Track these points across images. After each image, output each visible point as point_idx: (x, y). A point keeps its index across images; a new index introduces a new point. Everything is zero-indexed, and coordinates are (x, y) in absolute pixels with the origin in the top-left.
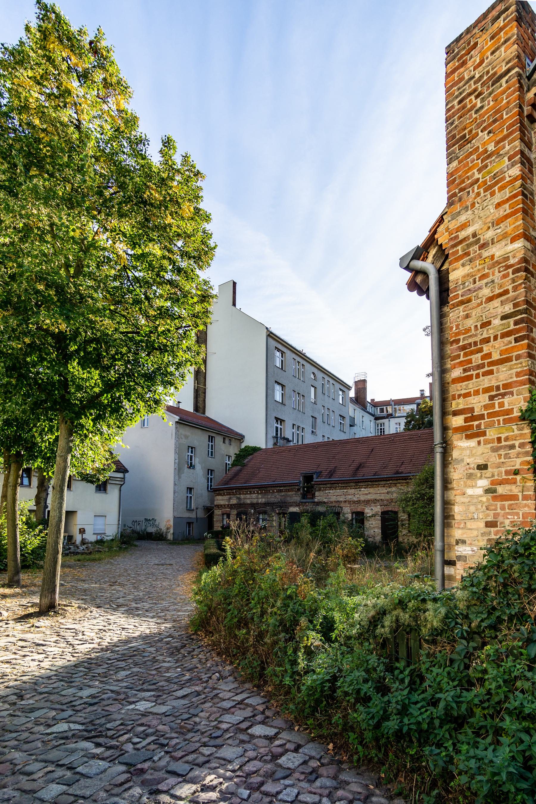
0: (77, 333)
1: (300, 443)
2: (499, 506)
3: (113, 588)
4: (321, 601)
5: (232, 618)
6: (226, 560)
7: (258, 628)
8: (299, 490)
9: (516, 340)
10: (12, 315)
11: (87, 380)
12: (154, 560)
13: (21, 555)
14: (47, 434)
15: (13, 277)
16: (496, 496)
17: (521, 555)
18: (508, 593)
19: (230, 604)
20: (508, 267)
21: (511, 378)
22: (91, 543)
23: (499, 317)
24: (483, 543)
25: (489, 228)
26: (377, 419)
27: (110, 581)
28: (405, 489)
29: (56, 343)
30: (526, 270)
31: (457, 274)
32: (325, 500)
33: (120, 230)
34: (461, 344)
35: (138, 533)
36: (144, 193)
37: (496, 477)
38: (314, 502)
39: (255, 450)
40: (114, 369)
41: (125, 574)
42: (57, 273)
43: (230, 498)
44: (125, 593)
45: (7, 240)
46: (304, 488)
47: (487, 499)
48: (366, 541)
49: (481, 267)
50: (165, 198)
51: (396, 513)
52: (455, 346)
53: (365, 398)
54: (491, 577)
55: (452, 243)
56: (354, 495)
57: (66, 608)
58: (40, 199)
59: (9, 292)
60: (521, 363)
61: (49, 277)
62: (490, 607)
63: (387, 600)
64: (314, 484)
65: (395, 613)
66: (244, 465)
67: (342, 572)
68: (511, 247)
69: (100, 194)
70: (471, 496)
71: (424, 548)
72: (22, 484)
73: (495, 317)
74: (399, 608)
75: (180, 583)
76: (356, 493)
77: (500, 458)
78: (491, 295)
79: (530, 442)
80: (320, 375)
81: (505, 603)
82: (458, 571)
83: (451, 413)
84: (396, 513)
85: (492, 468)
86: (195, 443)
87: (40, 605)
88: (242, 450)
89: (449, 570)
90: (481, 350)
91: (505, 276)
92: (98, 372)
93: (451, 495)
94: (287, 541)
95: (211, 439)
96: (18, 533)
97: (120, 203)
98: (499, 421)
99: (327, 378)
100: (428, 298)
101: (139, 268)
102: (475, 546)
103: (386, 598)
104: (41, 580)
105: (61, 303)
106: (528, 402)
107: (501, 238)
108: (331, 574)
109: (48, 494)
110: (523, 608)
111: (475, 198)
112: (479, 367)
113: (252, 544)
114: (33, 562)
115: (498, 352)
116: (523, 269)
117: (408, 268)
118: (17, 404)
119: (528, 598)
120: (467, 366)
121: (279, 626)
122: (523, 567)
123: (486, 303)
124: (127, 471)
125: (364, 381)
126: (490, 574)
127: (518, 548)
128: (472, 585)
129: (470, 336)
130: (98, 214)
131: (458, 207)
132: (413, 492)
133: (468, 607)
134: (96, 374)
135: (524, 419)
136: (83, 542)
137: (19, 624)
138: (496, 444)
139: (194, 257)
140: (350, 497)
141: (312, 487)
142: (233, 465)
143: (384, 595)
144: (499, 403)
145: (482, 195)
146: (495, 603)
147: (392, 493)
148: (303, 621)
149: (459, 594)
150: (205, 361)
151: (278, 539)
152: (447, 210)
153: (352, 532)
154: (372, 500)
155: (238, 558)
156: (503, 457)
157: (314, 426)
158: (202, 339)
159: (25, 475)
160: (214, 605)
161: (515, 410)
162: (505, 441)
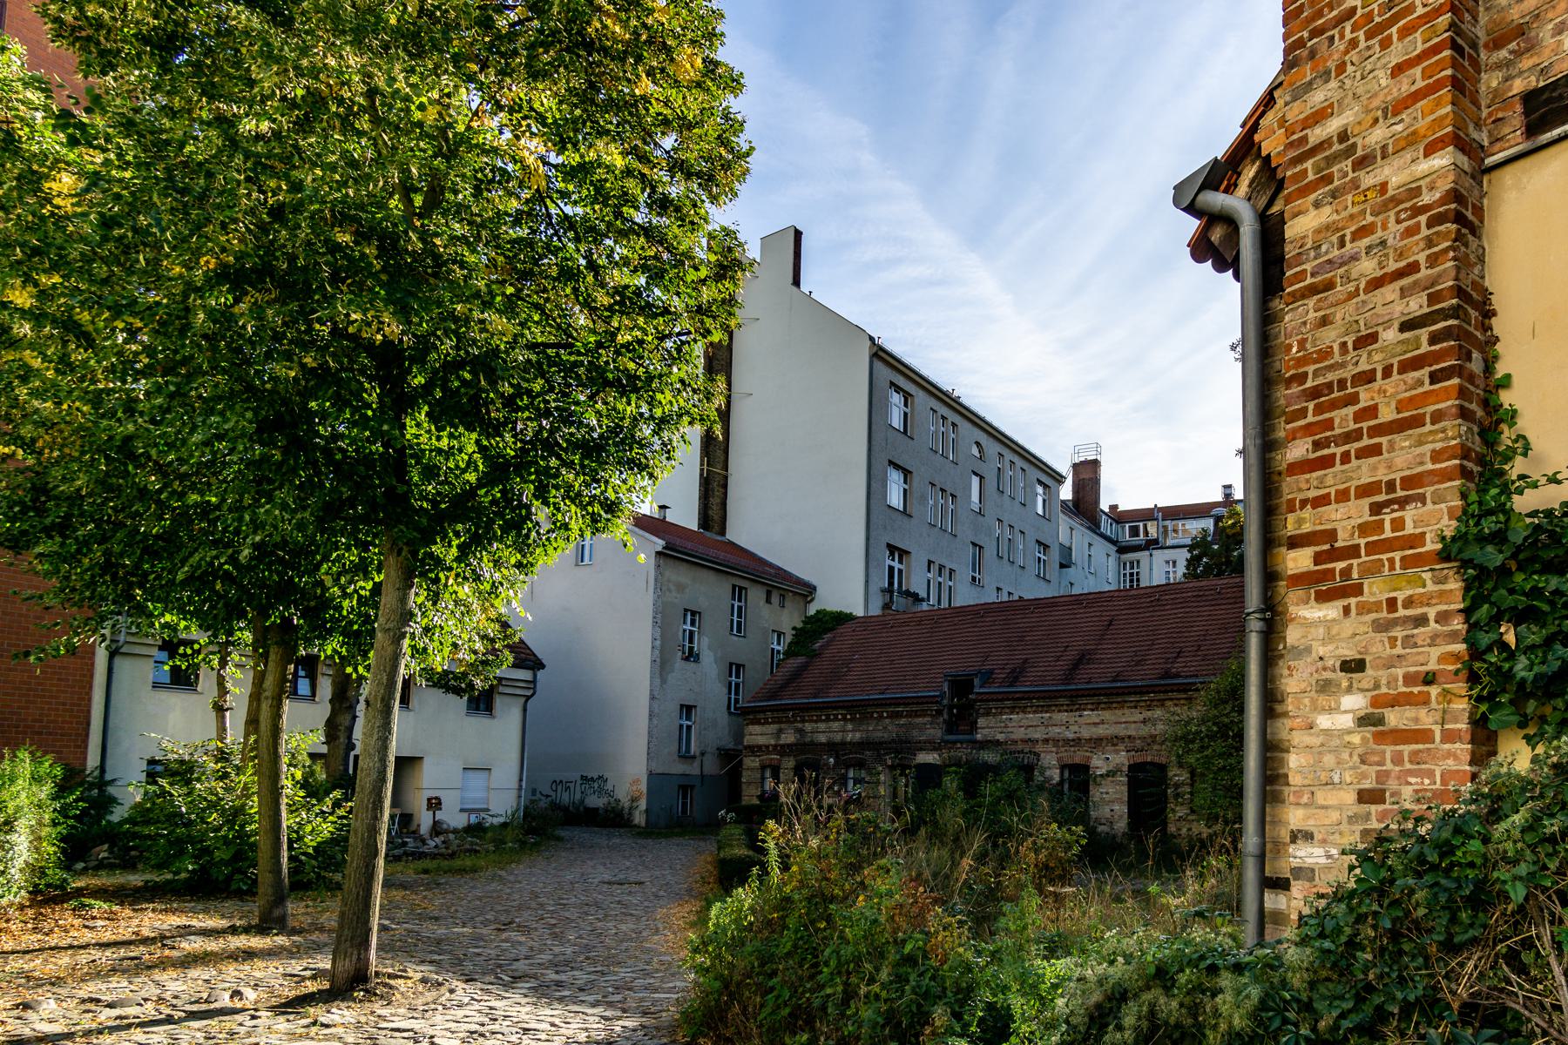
0: (424, 346)
1: (944, 604)
2: (1388, 756)
3: (504, 935)
4: (982, 969)
5: (779, 1007)
6: (768, 874)
7: (837, 1030)
8: (939, 712)
9: (1434, 378)
10: (275, 301)
11: (448, 454)
12: (599, 872)
13: (291, 858)
14: (351, 579)
15: (278, 212)
16: (1382, 733)
17: (1434, 868)
18: (1401, 953)
19: (774, 974)
20: (1417, 211)
21: (1422, 463)
22: (455, 831)
23: (1396, 325)
24: (1352, 837)
25: (1376, 121)
26: (1123, 550)
27: (496, 921)
28: (1184, 712)
29: (378, 369)
30: (1459, 218)
31: (1303, 224)
32: (1001, 737)
33: (532, 109)
34: (1309, 384)
35: (565, 809)
36: (589, 23)
37: (1384, 690)
38: (976, 742)
39: (842, 618)
40: (514, 428)
41: (534, 905)
42: (382, 206)
43: (780, 731)
44: (531, 948)
45: (265, 126)
46: (951, 707)
47: (1363, 739)
48: (1091, 832)
49: (1356, 209)
50: (636, 34)
51: (1163, 768)
52: (1295, 389)
53: (1097, 501)
54: (1366, 916)
55: (1292, 154)
56: (1067, 725)
57: (392, 982)
58: (344, 32)
59: (271, 249)
60: (1444, 431)
61: (364, 216)
62: (1360, 985)
63: (1131, 968)
64: (975, 701)
65: (1147, 997)
66: (815, 655)
67: (1032, 901)
68: (1424, 166)
69: (486, 24)
70: (1326, 732)
71: (1223, 850)
72: (295, 692)
73: (1387, 324)
74: (1156, 986)
75: (660, 926)
76: (1072, 720)
77: (1393, 646)
78: (1379, 273)
79: (1460, 611)
80: (992, 448)
81: (1394, 975)
82: (1294, 902)
83: (1284, 541)
84: (1163, 768)
85: (1376, 668)
86: (701, 603)
87: (331, 975)
88: (808, 620)
89: (1274, 901)
90: (1353, 399)
91: (1410, 232)
92: (474, 436)
93: (1288, 729)
94: (910, 832)
95: (738, 593)
96: (283, 808)
97: (531, 47)
98: (1391, 561)
99: (1009, 456)
100: (1237, 276)
101: (574, 197)
102: (1335, 845)
103: (1128, 963)
104: (335, 916)
105: (391, 275)
106: (1459, 520)
107: (1403, 143)
108: (1007, 907)
109: (355, 717)
110: (1434, 988)
111: (1347, 52)
112: (1349, 437)
113: (827, 838)
114: (318, 875)
115: (1393, 405)
116: (1452, 216)
117: (1191, 209)
118: (284, 507)
119: (1447, 965)
120: (1320, 433)
121: (883, 1027)
122: (1436, 894)
123: (1366, 291)
124: (541, 666)
125: (1095, 464)
126: (1364, 909)
127: (1427, 851)
128: (1322, 936)
129: (1331, 368)
130: (481, 70)
131: (1307, 72)
132: (1203, 721)
133: (1312, 985)
134: (470, 441)
135: (1447, 559)
136: (437, 828)
137: (282, 1019)
138: (1384, 614)
139: (699, 175)
141: (971, 705)
142: (789, 654)
143: (1124, 956)
144: (1393, 521)
145: (1362, 44)
146: (1371, 976)
147: (1154, 722)
148: (940, 1016)
149: (1292, 954)
150: (725, 415)
151: (887, 826)
152: (1282, 78)
153: (1059, 811)
154: (1107, 740)
155: (795, 868)
156: (1399, 643)
157: (977, 564)
158: (720, 361)
159: (302, 673)
160: (737, 978)
161: (1428, 536)
162: (1405, 607)
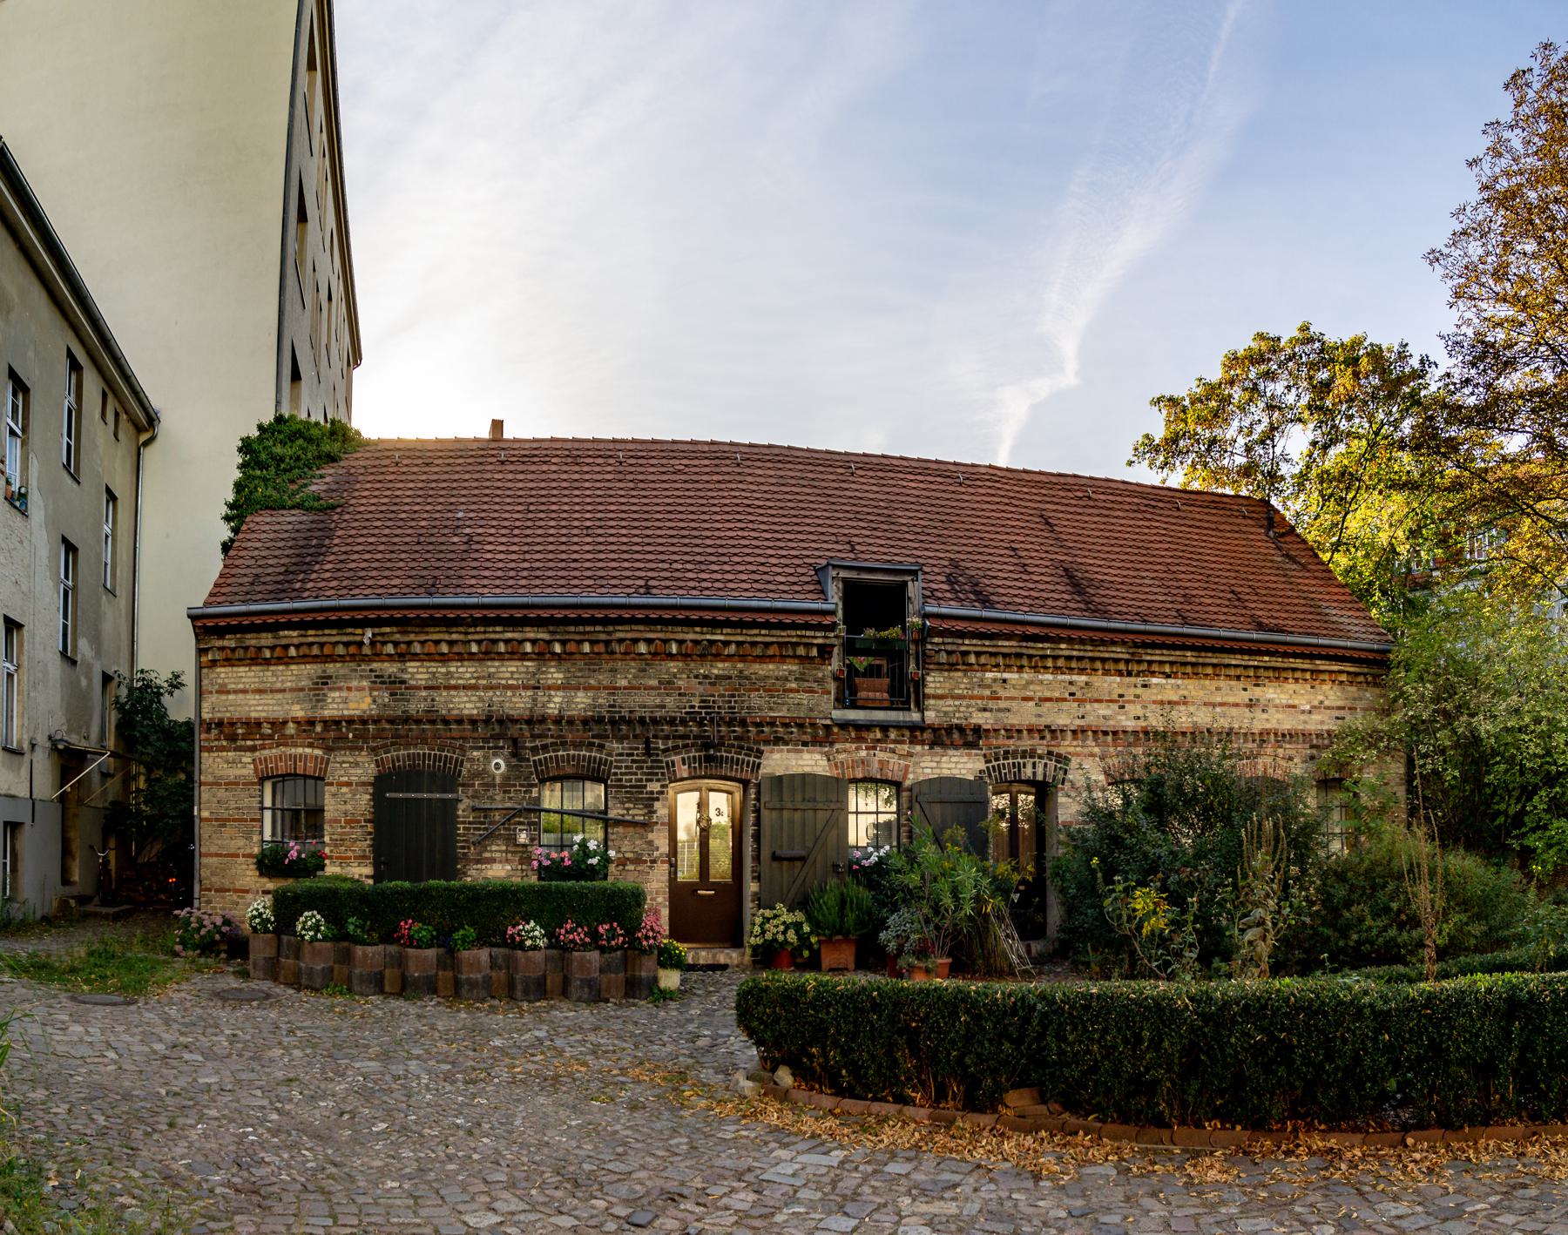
32: (979, 718)
43: (324, 681)
56: (1120, 702)
76: (1130, 693)
140: (1103, 710)
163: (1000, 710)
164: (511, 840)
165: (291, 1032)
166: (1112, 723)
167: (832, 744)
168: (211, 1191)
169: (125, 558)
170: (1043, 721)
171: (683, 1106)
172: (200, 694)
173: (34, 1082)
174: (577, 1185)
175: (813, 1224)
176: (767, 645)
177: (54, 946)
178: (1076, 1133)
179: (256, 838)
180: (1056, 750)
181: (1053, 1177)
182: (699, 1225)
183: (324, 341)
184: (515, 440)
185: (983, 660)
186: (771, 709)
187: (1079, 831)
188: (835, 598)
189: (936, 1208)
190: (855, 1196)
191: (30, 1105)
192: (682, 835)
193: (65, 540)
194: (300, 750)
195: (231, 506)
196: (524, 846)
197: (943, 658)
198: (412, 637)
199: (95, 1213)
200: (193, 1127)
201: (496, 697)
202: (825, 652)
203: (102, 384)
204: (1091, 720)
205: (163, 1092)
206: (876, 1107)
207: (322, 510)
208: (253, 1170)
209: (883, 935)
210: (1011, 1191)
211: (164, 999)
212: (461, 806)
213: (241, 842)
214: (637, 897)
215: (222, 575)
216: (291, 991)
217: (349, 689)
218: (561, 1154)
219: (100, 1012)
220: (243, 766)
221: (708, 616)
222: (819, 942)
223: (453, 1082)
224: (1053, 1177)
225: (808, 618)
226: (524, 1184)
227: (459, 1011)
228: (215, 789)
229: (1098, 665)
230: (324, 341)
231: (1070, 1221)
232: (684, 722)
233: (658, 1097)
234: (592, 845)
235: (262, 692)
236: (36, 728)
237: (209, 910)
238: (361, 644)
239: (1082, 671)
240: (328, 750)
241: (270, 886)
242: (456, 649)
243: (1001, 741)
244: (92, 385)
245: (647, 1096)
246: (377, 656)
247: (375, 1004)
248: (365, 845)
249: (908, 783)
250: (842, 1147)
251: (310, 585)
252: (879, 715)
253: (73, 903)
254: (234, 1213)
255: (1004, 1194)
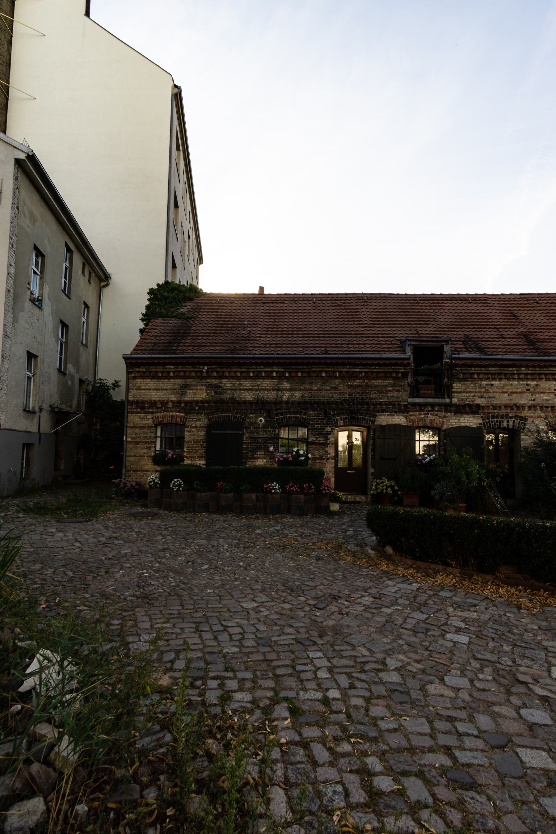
32: (478, 401)
140: (545, 397)
163: (490, 397)
164: (267, 450)
165: (166, 529)
166: (551, 402)
167: (408, 412)
168: (125, 599)
169: (92, 332)
170: (512, 402)
171: (340, 559)
172: (128, 390)
173: (35, 562)
174: (292, 591)
175: (406, 615)
176: (378, 372)
177: (49, 499)
178: (540, 590)
179: (153, 449)
180: (519, 415)
181: (527, 608)
182: (347, 610)
183: (187, 253)
184: (269, 294)
185: (481, 376)
186: (380, 398)
187: (533, 451)
188: (409, 352)
189: (466, 614)
190: (425, 604)
191: (32, 572)
192: (340, 449)
193: (61, 322)
194: (174, 414)
195: (144, 315)
196: (272, 452)
197: (461, 376)
198: (225, 370)
199: (65, 616)
200: (118, 572)
201: (261, 393)
202: (405, 375)
203: (83, 260)
204: (539, 401)
205: (103, 558)
206: (433, 566)
207: (186, 319)
208: (146, 588)
209: (432, 492)
210: (505, 612)
211: (106, 518)
212: (245, 436)
213: (146, 451)
214: (321, 473)
215: (139, 342)
216: (167, 512)
217: (197, 390)
218: (286, 577)
219: (72, 526)
220: (149, 420)
221: (352, 361)
222: (402, 494)
223: (239, 548)
224: (527, 608)
225: (397, 362)
226: (269, 590)
227: (242, 518)
228: (134, 429)
229: (543, 376)
230: (187, 253)
231: (540, 632)
232: (341, 403)
233: (329, 555)
234: (301, 452)
235: (152, 390)
236: (43, 402)
237: (130, 479)
238: (202, 372)
239: (533, 380)
240: (187, 414)
241: (159, 469)
242: (243, 375)
243: (490, 411)
244: (78, 261)
245: (324, 555)
246: (209, 377)
247: (205, 517)
248: (202, 452)
249: (444, 428)
250: (418, 582)
251: (180, 348)
252: (430, 400)
253: (60, 479)
254: (135, 608)
255: (502, 613)
